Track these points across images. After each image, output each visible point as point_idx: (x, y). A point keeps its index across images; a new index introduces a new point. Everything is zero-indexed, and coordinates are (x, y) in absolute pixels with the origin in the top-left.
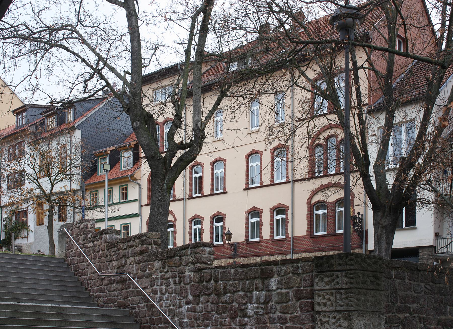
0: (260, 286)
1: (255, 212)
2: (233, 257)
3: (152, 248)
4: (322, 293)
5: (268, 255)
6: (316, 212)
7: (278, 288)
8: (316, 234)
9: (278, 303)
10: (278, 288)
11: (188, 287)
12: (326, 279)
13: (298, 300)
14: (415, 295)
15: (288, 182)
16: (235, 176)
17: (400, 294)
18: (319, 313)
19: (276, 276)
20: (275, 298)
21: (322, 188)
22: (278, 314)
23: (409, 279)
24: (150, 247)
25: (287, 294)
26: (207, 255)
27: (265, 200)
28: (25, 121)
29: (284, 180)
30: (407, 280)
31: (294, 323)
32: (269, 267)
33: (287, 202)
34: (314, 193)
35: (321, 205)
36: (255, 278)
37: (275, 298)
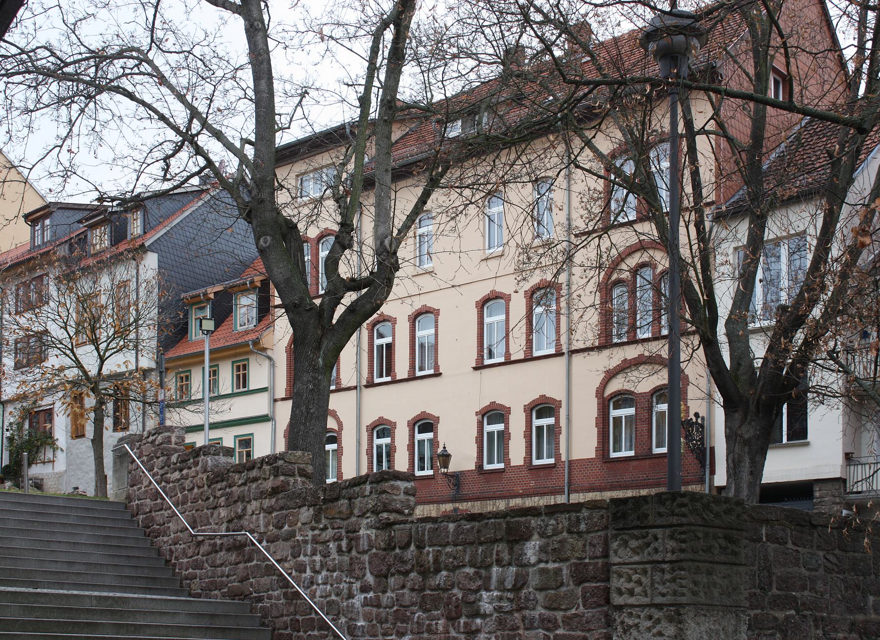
0: (506, 557)
1: (496, 413)
2: (454, 500)
3: (296, 482)
4: (625, 569)
5: (521, 496)
6: (614, 413)
7: (540, 561)
8: (613, 455)
9: (541, 590)
10: (540, 561)
11: (366, 558)
12: (634, 543)
13: (578, 583)
14: (807, 573)
15: (559, 354)
16: (456, 343)
17: (778, 571)
18: (619, 608)
19: (536, 536)
20: (534, 580)
21: (626, 366)
22: (540, 610)
23: (794, 544)
24: (292, 480)
25: (558, 571)
26: (402, 497)
27: (515, 388)
28: (48, 235)
29: (552, 351)
30: (790, 545)
31: (571, 629)
32: (523, 519)
33: (557, 393)
34: (611, 375)
35: (623, 398)
36: (496, 541)
37: (534, 580)
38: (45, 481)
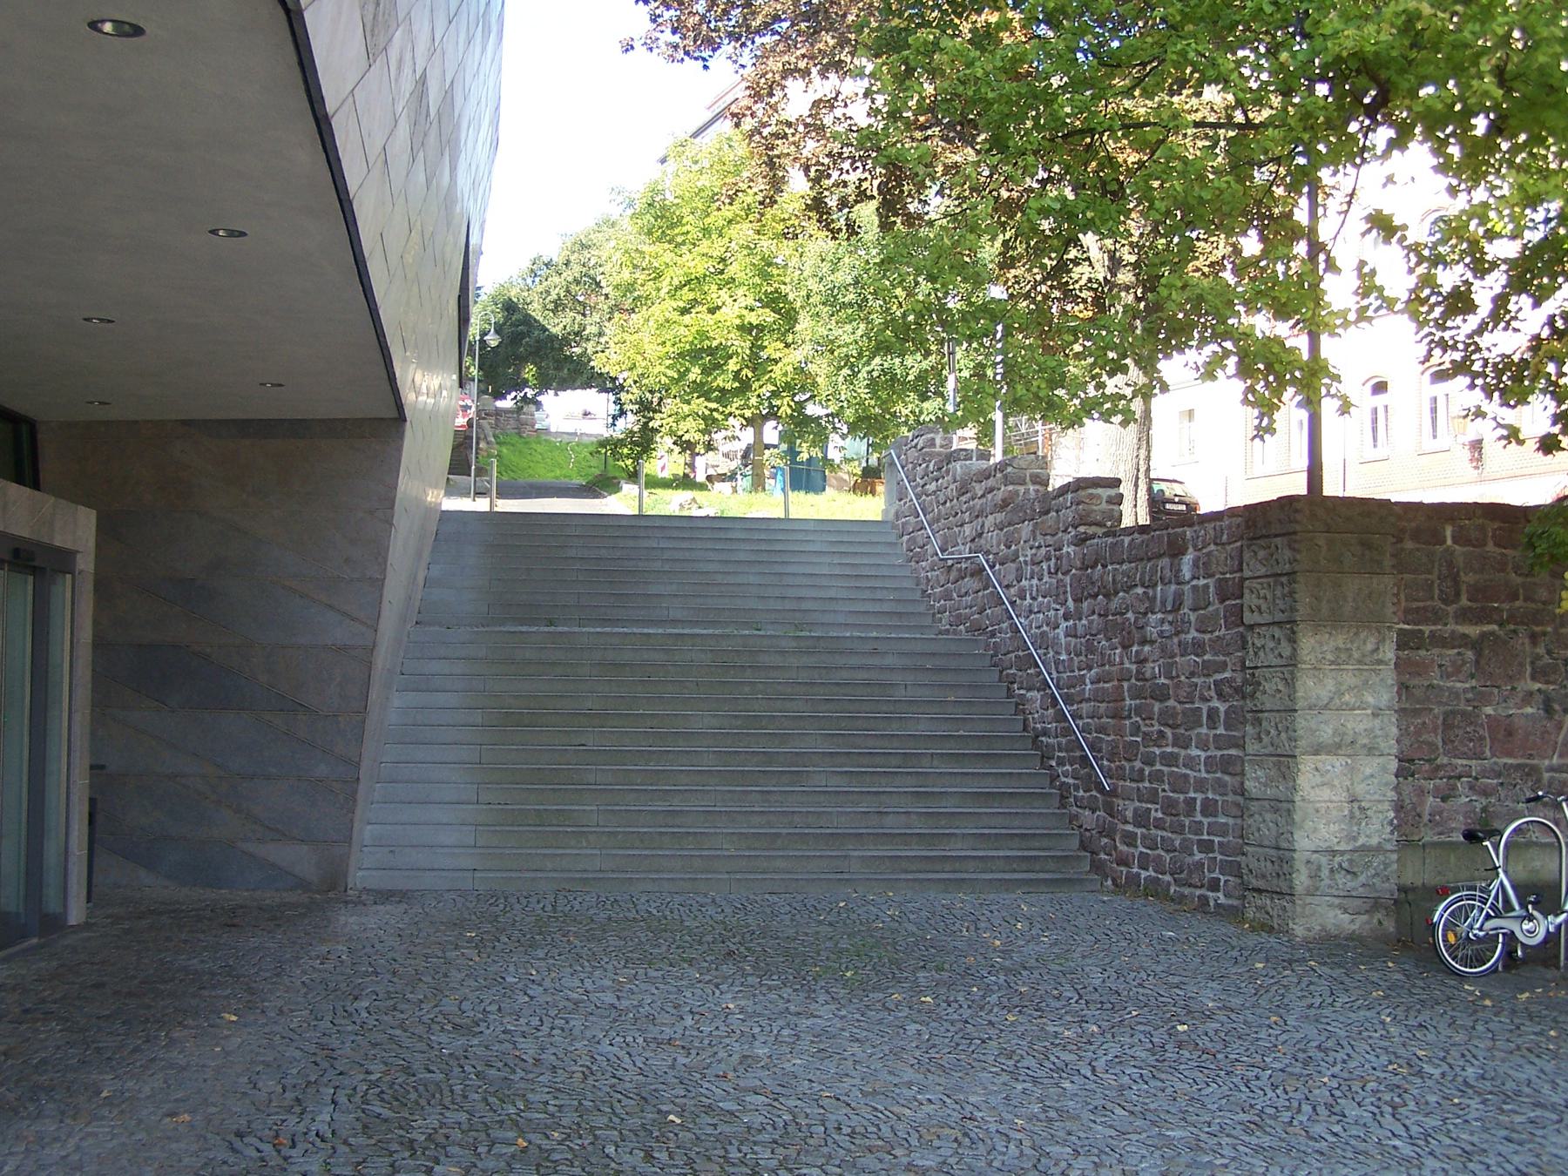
0: (1167, 573)
3: (1027, 491)
4: (1255, 584)
7: (1194, 578)
9: (1194, 610)
10: (1194, 578)
11: (1068, 579)
12: (1261, 554)
13: (1222, 601)
14: (1519, 580)
17: (1468, 578)
18: (1251, 627)
19: (1191, 550)
20: (1188, 600)
22: (1193, 633)
23: (1497, 545)
24: (1022, 489)
25: (1206, 586)
26: (1104, 506)
30: (1490, 547)
31: (1216, 654)
32: (1179, 530)
36: (1160, 556)
37: (1188, 600)
38: (79, 556)
